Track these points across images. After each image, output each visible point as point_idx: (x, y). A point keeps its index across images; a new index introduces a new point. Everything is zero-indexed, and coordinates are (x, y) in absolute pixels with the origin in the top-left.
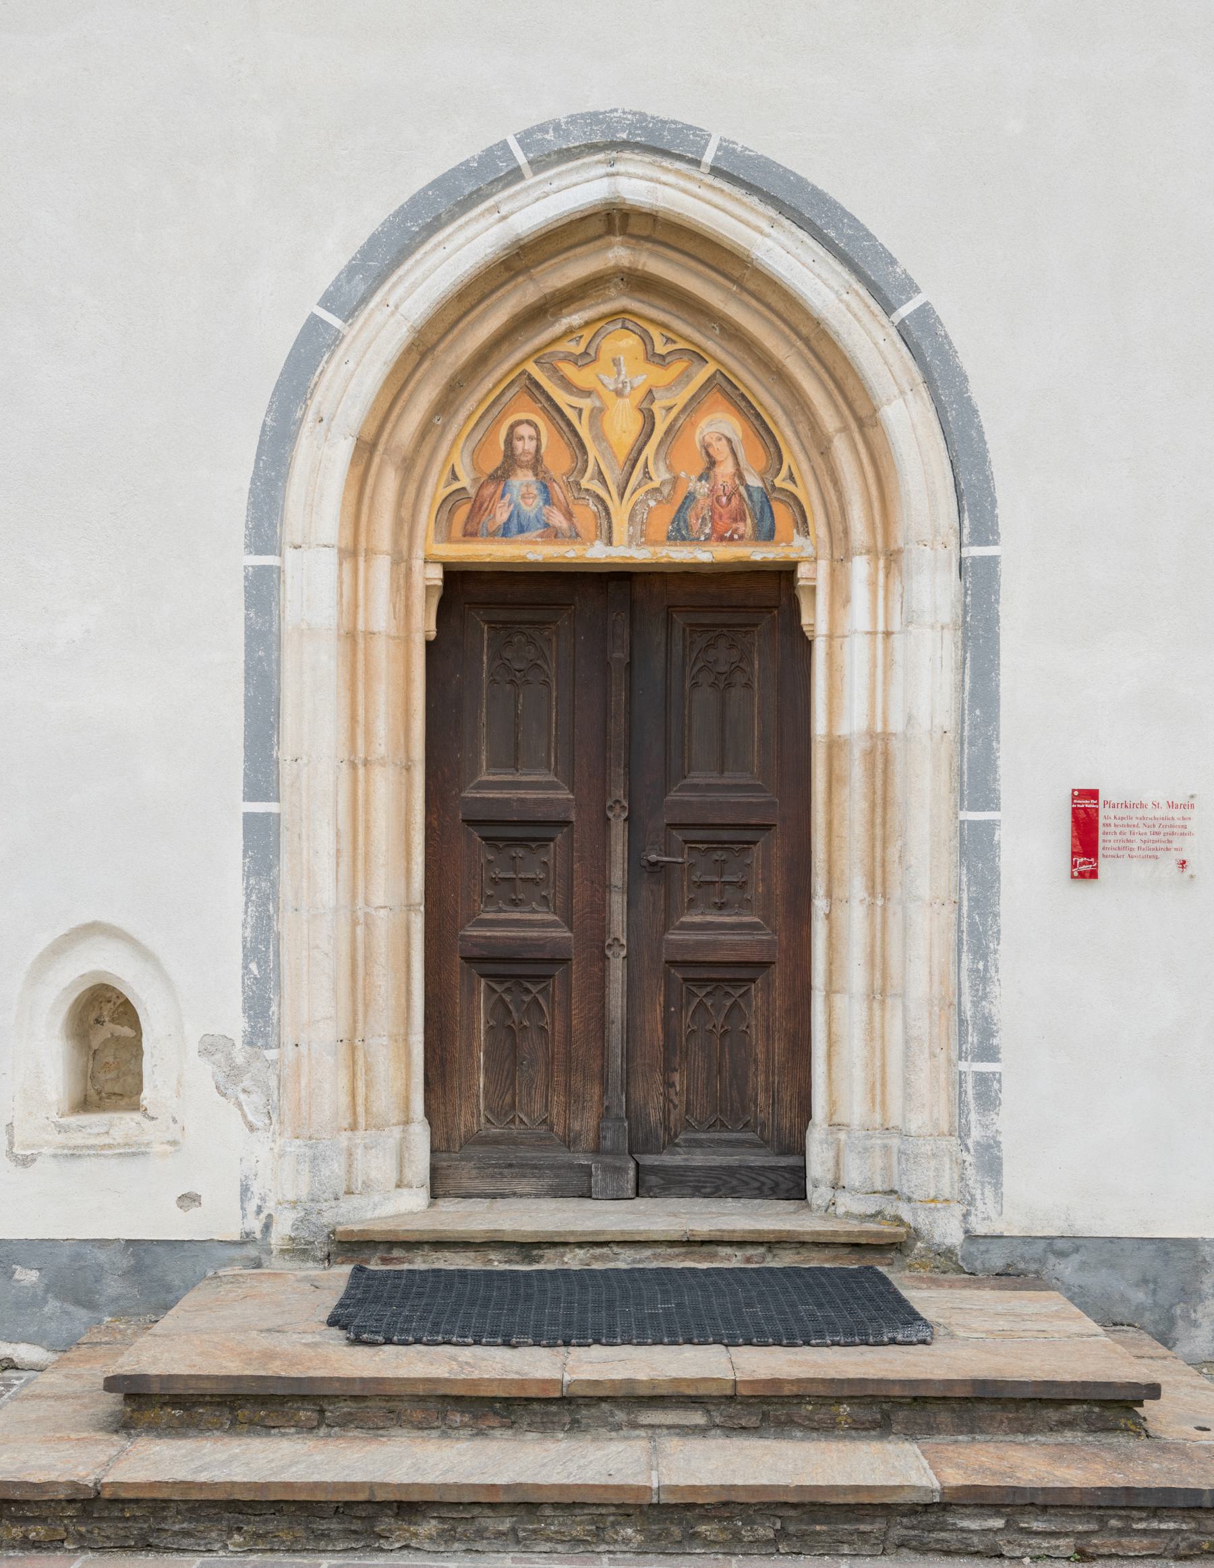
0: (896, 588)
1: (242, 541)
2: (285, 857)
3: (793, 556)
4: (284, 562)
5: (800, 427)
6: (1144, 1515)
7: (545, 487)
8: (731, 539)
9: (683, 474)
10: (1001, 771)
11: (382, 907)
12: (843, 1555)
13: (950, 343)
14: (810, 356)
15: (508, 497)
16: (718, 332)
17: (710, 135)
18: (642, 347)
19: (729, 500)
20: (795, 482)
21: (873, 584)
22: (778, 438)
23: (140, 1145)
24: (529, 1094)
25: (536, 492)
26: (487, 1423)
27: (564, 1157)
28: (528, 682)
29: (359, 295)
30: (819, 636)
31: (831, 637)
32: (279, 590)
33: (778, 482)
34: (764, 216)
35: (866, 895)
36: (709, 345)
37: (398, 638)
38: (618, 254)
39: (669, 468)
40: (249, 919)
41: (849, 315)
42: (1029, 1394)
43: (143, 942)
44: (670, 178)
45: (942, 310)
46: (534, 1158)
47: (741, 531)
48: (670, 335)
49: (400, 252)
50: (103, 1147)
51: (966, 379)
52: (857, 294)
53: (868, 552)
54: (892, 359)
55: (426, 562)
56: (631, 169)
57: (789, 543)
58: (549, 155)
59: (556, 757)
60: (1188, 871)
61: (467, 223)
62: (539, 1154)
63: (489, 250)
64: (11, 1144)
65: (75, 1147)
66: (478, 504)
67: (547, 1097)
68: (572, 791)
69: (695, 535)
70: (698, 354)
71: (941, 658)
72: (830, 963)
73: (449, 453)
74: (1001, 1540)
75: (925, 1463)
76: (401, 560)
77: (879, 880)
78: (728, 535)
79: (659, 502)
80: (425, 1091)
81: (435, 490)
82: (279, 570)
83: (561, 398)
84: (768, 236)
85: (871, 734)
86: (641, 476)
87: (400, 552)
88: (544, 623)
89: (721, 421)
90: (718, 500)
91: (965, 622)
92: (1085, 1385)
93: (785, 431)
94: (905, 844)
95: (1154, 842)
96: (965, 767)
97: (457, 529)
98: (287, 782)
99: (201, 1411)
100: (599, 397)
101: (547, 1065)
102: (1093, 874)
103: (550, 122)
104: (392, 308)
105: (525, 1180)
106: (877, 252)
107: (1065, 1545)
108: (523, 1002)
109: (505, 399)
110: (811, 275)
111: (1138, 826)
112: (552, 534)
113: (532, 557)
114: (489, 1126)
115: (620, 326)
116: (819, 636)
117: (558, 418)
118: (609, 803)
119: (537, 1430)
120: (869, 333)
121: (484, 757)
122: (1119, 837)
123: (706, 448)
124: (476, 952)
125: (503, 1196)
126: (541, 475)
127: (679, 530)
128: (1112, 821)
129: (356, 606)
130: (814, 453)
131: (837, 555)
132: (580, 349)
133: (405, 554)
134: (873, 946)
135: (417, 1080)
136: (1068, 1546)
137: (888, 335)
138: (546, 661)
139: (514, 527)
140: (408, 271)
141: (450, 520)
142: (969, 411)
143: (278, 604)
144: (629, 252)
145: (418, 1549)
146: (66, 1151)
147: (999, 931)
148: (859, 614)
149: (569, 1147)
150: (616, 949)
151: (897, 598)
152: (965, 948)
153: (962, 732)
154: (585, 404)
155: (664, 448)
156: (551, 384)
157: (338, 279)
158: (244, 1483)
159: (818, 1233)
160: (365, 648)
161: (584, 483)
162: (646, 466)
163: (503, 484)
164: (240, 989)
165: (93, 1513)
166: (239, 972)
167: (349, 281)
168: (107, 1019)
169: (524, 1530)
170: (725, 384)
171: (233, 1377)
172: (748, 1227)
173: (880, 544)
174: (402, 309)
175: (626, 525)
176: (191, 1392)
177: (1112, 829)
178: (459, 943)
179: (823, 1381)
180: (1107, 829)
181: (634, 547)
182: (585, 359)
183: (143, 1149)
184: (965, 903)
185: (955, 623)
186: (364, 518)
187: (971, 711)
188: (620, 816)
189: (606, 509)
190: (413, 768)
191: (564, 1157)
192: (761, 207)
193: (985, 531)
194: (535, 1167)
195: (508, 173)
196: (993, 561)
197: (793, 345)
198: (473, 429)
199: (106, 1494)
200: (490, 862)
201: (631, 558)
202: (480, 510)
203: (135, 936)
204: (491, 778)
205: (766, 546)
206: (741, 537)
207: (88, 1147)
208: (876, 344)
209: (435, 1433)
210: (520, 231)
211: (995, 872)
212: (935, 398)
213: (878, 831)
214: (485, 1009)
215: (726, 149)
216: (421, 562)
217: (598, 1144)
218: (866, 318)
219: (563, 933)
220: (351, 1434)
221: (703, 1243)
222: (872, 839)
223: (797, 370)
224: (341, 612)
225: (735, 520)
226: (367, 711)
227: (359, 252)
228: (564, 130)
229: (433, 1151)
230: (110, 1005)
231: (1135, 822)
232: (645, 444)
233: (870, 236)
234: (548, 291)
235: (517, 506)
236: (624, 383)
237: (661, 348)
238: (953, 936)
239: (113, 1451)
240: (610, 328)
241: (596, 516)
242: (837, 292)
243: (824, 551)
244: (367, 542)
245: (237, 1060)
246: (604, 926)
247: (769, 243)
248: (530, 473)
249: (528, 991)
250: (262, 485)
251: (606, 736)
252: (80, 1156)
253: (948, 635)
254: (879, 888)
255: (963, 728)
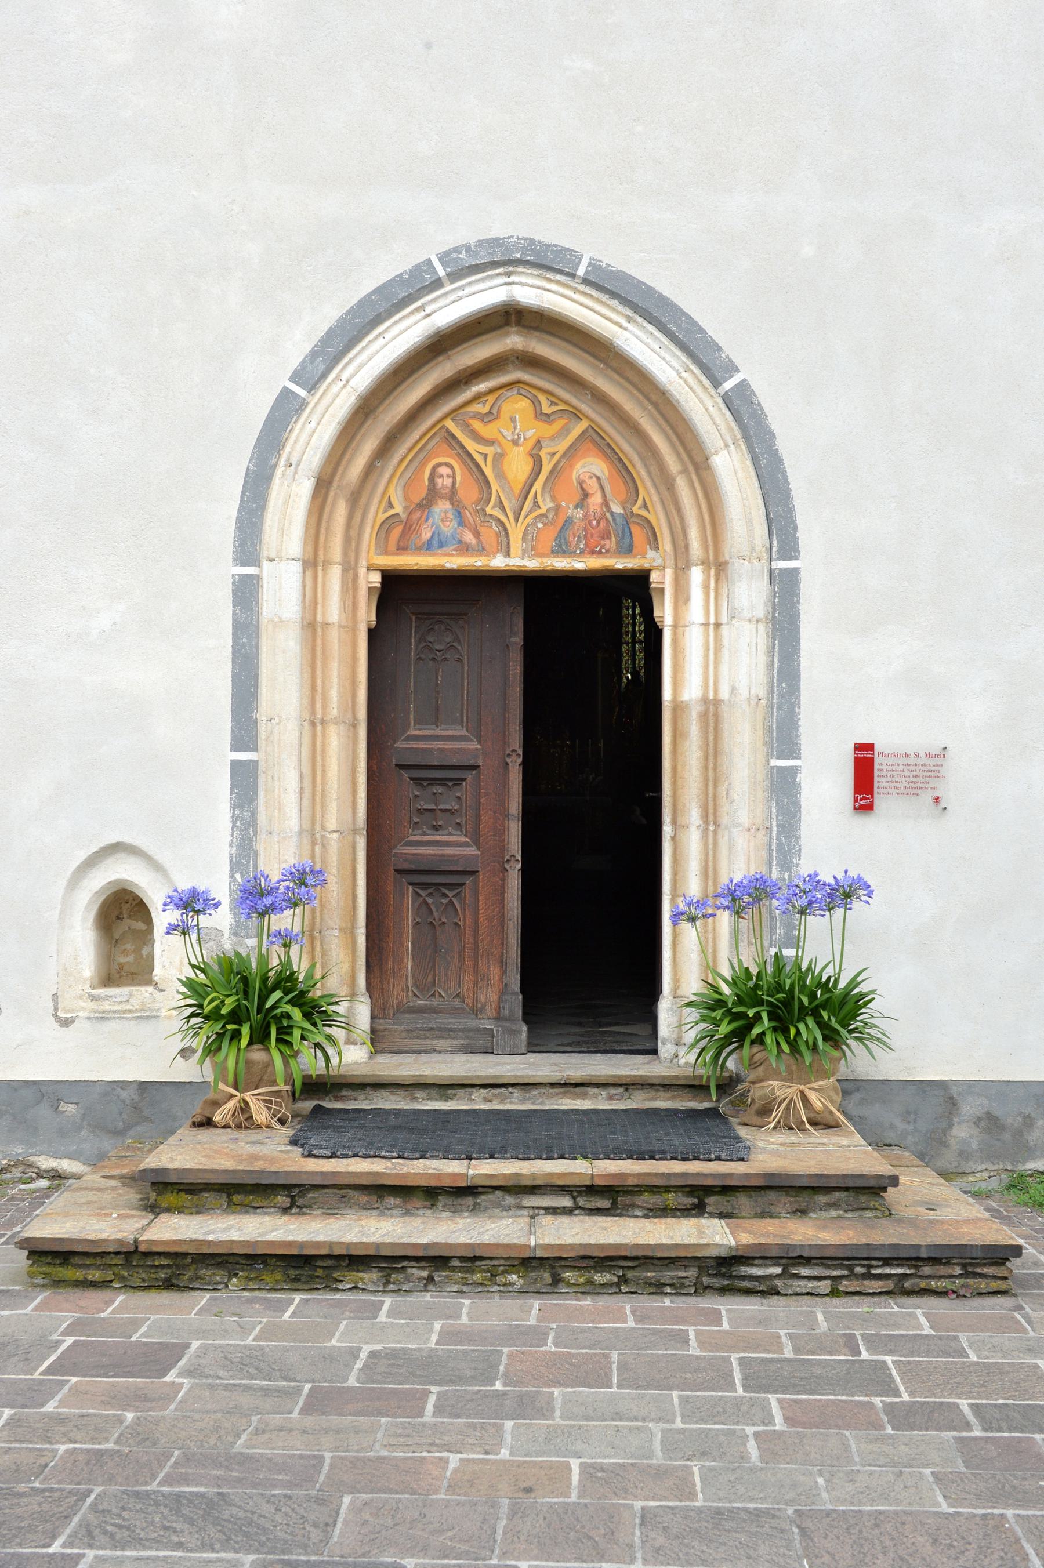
0: (724, 591)
1: (230, 556)
2: (261, 793)
3: (647, 566)
4: (262, 571)
5: (652, 468)
6: (880, 1263)
7: (459, 513)
8: (600, 552)
9: (563, 504)
10: (802, 730)
11: (335, 832)
12: (667, 1293)
13: (762, 409)
14: (658, 416)
15: (431, 520)
16: (589, 397)
17: (582, 255)
18: (532, 409)
19: (598, 523)
20: (648, 510)
21: (706, 587)
22: (635, 477)
23: (152, 1010)
24: (446, 975)
25: (452, 517)
26: (414, 1205)
27: (473, 1023)
28: (446, 659)
29: (320, 372)
30: (667, 626)
31: (675, 627)
32: (258, 593)
33: (635, 509)
34: (622, 314)
35: (701, 822)
36: (583, 407)
37: (347, 627)
38: (514, 340)
39: (553, 499)
40: (235, 840)
41: (687, 388)
42: (805, 1183)
43: (155, 858)
44: (553, 287)
45: (757, 385)
46: (449, 1023)
47: (607, 547)
48: (554, 399)
49: (350, 341)
50: (125, 1012)
51: (774, 436)
52: (693, 372)
53: (703, 563)
54: (719, 420)
55: (368, 570)
56: (523, 279)
57: (644, 555)
58: (462, 269)
59: (467, 717)
60: (943, 805)
61: (401, 319)
62: (454, 1021)
63: (417, 339)
64: (56, 1009)
65: (104, 1012)
66: (408, 525)
67: (460, 977)
68: (479, 743)
69: (572, 549)
70: (575, 414)
71: (757, 644)
72: (675, 874)
73: (387, 487)
74: (779, 1283)
75: (728, 1231)
76: (349, 569)
77: (711, 811)
78: (597, 549)
79: (545, 524)
80: (367, 972)
81: (375, 515)
82: (257, 578)
83: (471, 446)
84: (625, 329)
85: (705, 700)
86: (531, 505)
87: (349, 562)
88: (461, 614)
89: (592, 464)
90: (590, 523)
91: (774, 616)
92: (845, 1176)
93: (640, 471)
94: (730, 784)
95: (915, 783)
96: (774, 726)
97: (392, 545)
98: (263, 737)
99: (206, 1195)
100: (500, 445)
101: (460, 952)
102: (870, 807)
103: (463, 246)
104: (344, 382)
105: (443, 1040)
106: (707, 342)
107: (825, 1286)
108: (442, 903)
109: (429, 447)
110: (658, 358)
111: (903, 771)
112: (464, 549)
113: (448, 566)
114: (415, 999)
115: (516, 392)
116: (667, 626)
117: (469, 461)
118: (508, 751)
119: (449, 1210)
120: (701, 401)
121: (412, 717)
122: (889, 779)
123: (581, 483)
124: (406, 866)
125: (426, 1052)
126: (456, 504)
127: (560, 546)
128: (884, 767)
129: (316, 604)
130: (662, 488)
131: (680, 565)
132: (486, 410)
133: (353, 563)
134: (706, 861)
135: (360, 963)
136: (826, 1285)
137: (716, 402)
138: (459, 643)
139: (435, 543)
140: (357, 355)
141: (387, 538)
142: (777, 460)
143: (257, 603)
144: (522, 339)
145: (363, 1289)
146: (97, 1015)
147: (800, 850)
148: (696, 610)
149: (477, 1015)
150: (513, 863)
151: (725, 597)
152: (775, 863)
153: (772, 700)
154: (489, 450)
155: (549, 484)
156: (464, 436)
157: (304, 361)
158: (240, 1242)
159: (664, 1077)
160: (323, 635)
161: (489, 510)
162: (535, 497)
163: (427, 510)
164: (228, 893)
165: (132, 1262)
166: (226, 879)
167: (312, 363)
168: (125, 916)
169: (439, 1276)
170: (595, 436)
171: (230, 1171)
172: (610, 1073)
173: (711, 558)
174: (352, 383)
175: (520, 541)
176: (199, 1181)
177: (885, 773)
178: (393, 859)
179: (656, 1174)
180: (880, 773)
181: (526, 559)
182: (489, 417)
183: (154, 1013)
184: (775, 829)
185: (767, 618)
186: (322, 538)
187: (779, 684)
188: (516, 762)
189: (507, 533)
190: (358, 726)
191: (473, 1023)
192: (621, 308)
193: (789, 548)
194: (450, 1030)
195: (432, 283)
196: (795, 571)
197: (646, 409)
198: (405, 470)
199: (142, 1248)
200: (416, 796)
201: (524, 566)
202: (409, 530)
203: (150, 853)
204: (417, 733)
205: (626, 558)
206: (607, 551)
207: (114, 1012)
208: (707, 409)
209: (375, 1213)
210: (440, 325)
211: (797, 806)
212: (751, 450)
213: (711, 774)
214: (412, 911)
215: (594, 265)
216: (364, 570)
217: (499, 1013)
218: (699, 390)
219: (472, 851)
220: (315, 1213)
221: (577, 1085)
222: (706, 780)
223: (649, 427)
224: (304, 608)
225: (603, 538)
226: (323, 682)
227: (319, 341)
228: (473, 251)
229: (373, 1017)
230: (128, 905)
231: (901, 768)
232: (535, 481)
233: (702, 331)
234: (461, 368)
235: (438, 527)
236: (519, 435)
237: (546, 409)
238: (764, 853)
239: (145, 1222)
240: (509, 394)
241: (498, 535)
242: (677, 371)
243: (670, 562)
244: (324, 555)
245: (225, 946)
246: (504, 846)
247: (626, 334)
248: (448, 503)
249: (445, 895)
250: (246, 513)
251: (505, 701)
252: (107, 1018)
253: (762, 627)
254: (711, 817)
255: (773, 697)
